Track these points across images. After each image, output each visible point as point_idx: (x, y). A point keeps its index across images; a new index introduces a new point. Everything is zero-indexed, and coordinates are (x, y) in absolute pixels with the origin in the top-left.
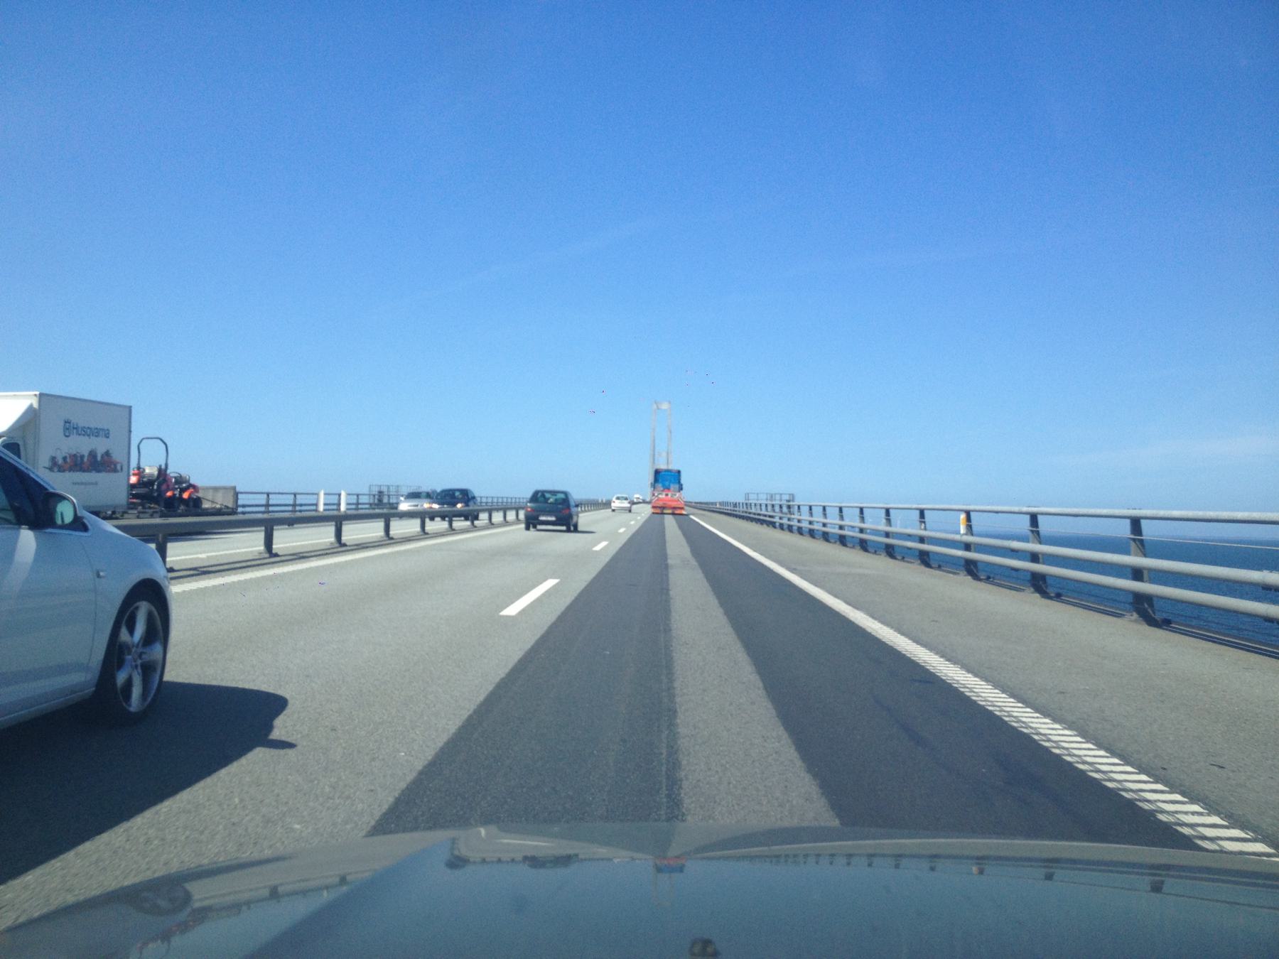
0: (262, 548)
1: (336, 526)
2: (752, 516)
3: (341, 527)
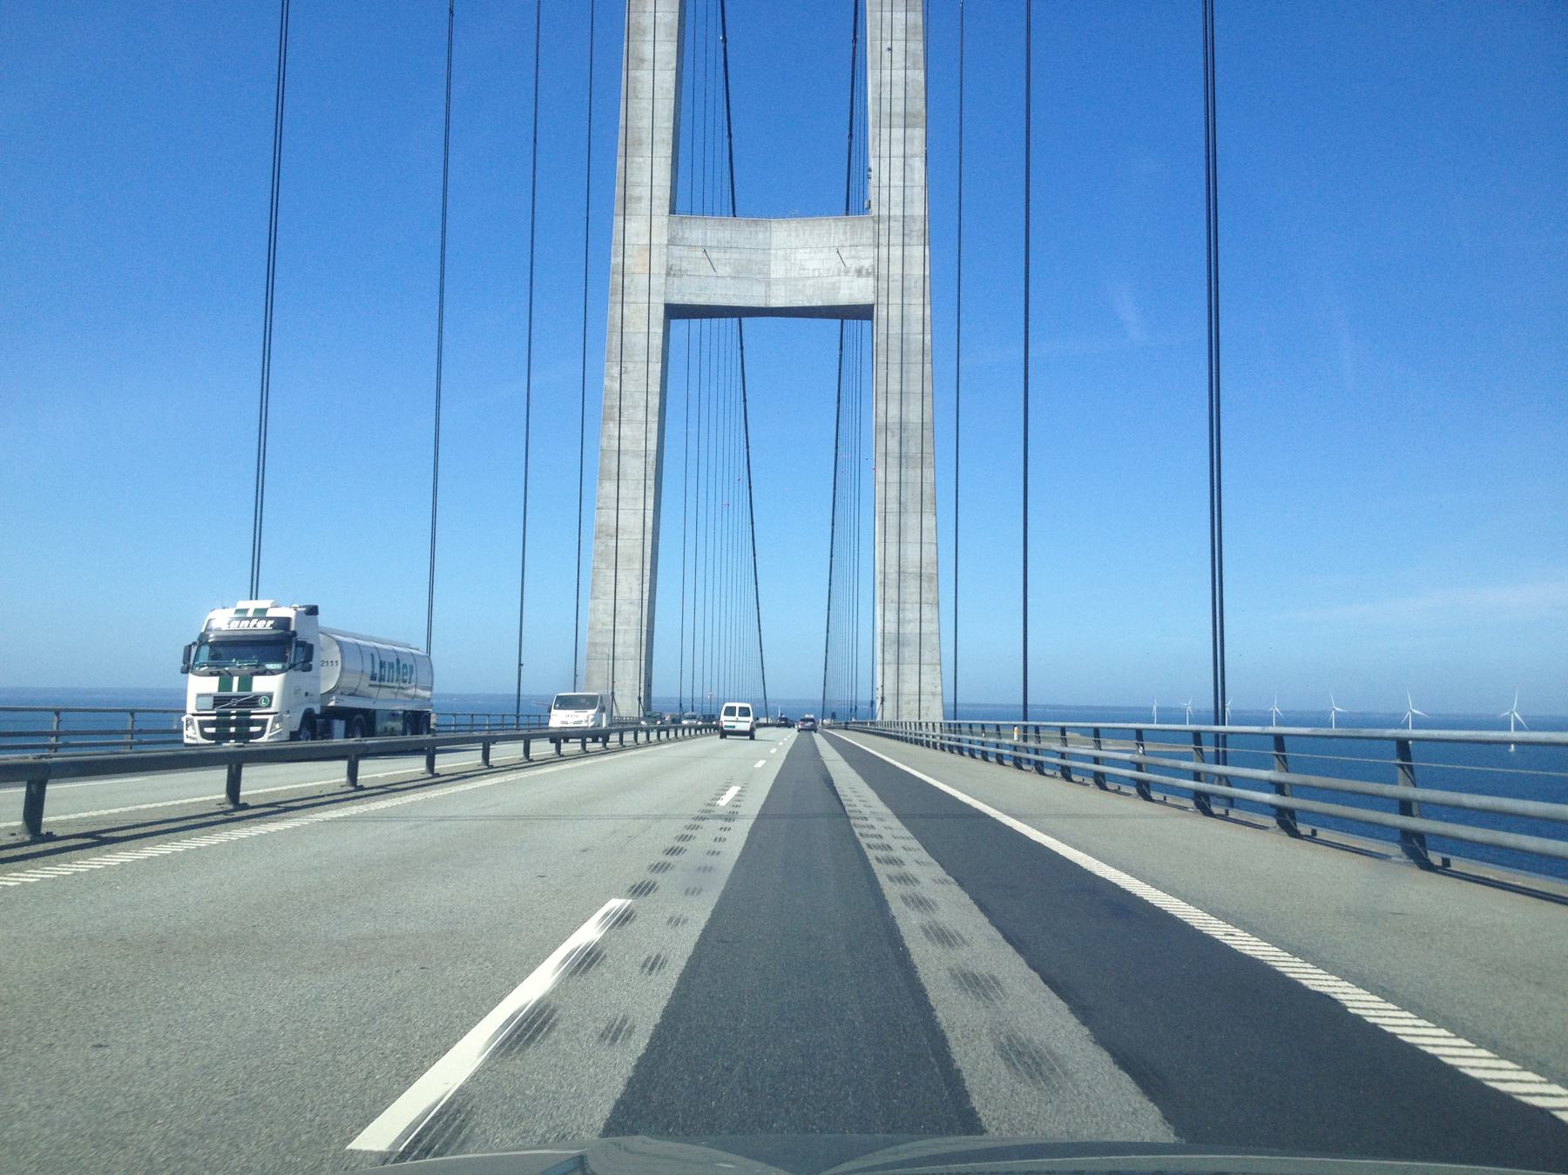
0: (344, 779)
1: (525, 742)
2: (892, 733)
3: (529, 742)
